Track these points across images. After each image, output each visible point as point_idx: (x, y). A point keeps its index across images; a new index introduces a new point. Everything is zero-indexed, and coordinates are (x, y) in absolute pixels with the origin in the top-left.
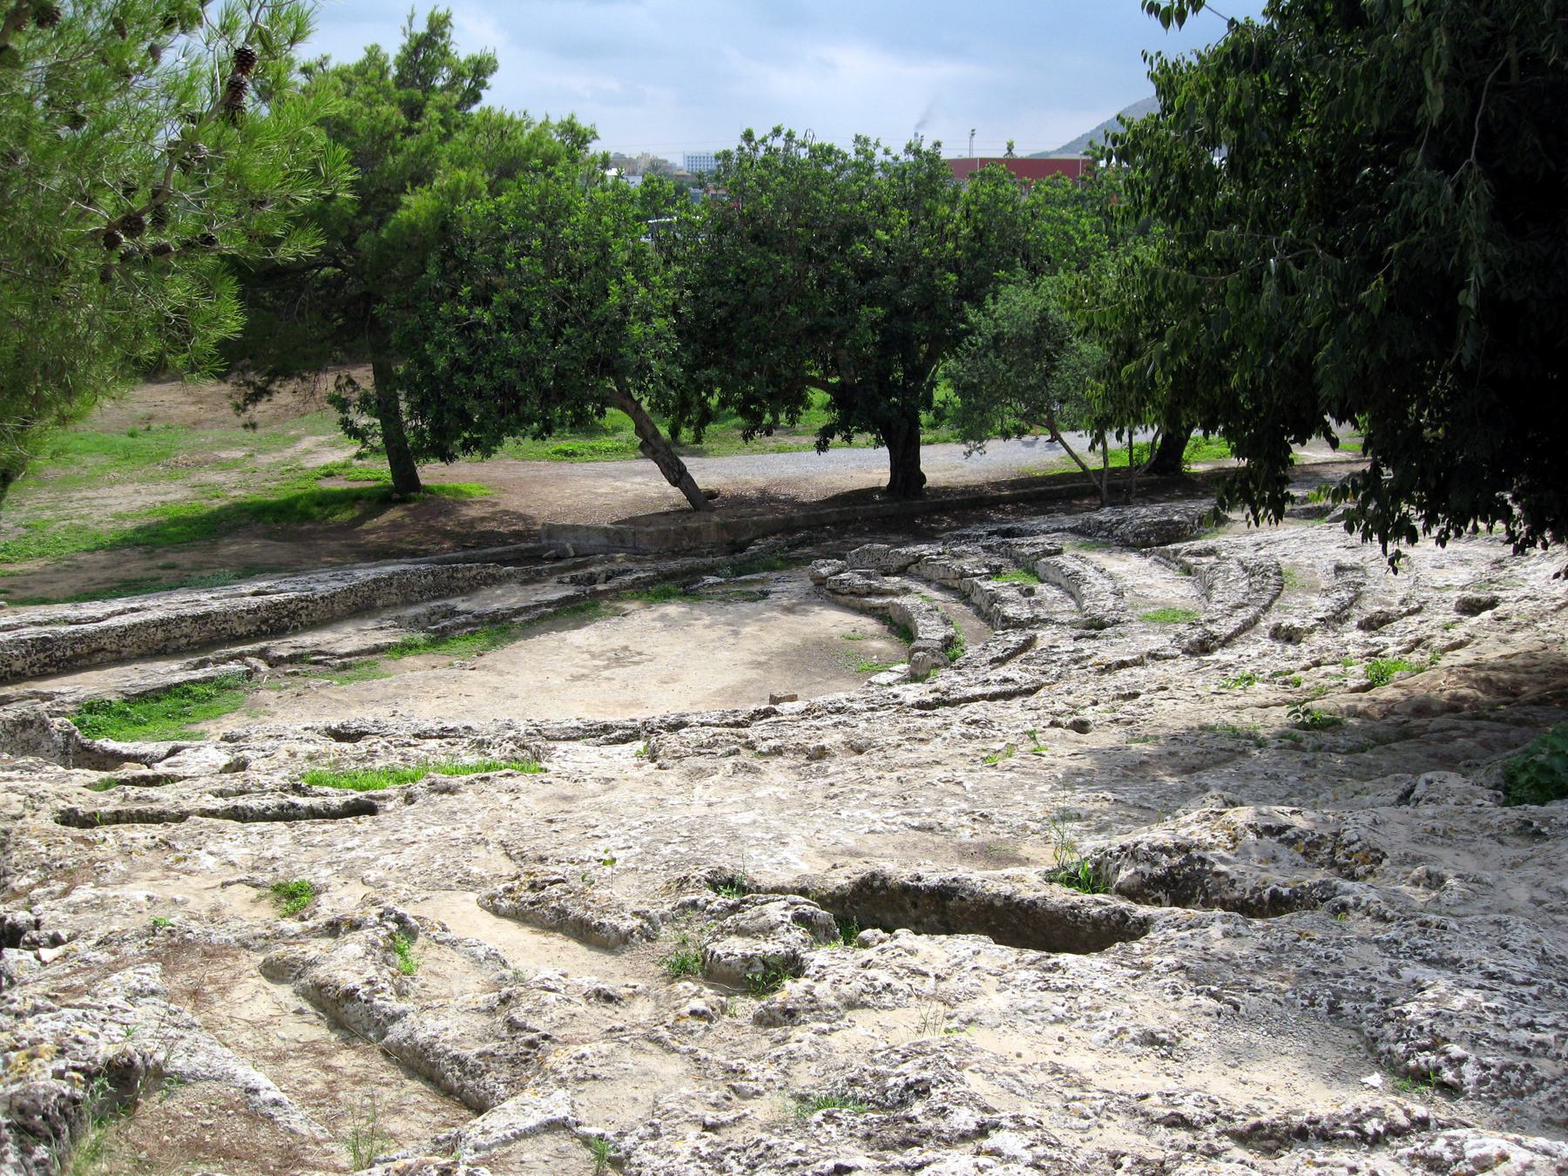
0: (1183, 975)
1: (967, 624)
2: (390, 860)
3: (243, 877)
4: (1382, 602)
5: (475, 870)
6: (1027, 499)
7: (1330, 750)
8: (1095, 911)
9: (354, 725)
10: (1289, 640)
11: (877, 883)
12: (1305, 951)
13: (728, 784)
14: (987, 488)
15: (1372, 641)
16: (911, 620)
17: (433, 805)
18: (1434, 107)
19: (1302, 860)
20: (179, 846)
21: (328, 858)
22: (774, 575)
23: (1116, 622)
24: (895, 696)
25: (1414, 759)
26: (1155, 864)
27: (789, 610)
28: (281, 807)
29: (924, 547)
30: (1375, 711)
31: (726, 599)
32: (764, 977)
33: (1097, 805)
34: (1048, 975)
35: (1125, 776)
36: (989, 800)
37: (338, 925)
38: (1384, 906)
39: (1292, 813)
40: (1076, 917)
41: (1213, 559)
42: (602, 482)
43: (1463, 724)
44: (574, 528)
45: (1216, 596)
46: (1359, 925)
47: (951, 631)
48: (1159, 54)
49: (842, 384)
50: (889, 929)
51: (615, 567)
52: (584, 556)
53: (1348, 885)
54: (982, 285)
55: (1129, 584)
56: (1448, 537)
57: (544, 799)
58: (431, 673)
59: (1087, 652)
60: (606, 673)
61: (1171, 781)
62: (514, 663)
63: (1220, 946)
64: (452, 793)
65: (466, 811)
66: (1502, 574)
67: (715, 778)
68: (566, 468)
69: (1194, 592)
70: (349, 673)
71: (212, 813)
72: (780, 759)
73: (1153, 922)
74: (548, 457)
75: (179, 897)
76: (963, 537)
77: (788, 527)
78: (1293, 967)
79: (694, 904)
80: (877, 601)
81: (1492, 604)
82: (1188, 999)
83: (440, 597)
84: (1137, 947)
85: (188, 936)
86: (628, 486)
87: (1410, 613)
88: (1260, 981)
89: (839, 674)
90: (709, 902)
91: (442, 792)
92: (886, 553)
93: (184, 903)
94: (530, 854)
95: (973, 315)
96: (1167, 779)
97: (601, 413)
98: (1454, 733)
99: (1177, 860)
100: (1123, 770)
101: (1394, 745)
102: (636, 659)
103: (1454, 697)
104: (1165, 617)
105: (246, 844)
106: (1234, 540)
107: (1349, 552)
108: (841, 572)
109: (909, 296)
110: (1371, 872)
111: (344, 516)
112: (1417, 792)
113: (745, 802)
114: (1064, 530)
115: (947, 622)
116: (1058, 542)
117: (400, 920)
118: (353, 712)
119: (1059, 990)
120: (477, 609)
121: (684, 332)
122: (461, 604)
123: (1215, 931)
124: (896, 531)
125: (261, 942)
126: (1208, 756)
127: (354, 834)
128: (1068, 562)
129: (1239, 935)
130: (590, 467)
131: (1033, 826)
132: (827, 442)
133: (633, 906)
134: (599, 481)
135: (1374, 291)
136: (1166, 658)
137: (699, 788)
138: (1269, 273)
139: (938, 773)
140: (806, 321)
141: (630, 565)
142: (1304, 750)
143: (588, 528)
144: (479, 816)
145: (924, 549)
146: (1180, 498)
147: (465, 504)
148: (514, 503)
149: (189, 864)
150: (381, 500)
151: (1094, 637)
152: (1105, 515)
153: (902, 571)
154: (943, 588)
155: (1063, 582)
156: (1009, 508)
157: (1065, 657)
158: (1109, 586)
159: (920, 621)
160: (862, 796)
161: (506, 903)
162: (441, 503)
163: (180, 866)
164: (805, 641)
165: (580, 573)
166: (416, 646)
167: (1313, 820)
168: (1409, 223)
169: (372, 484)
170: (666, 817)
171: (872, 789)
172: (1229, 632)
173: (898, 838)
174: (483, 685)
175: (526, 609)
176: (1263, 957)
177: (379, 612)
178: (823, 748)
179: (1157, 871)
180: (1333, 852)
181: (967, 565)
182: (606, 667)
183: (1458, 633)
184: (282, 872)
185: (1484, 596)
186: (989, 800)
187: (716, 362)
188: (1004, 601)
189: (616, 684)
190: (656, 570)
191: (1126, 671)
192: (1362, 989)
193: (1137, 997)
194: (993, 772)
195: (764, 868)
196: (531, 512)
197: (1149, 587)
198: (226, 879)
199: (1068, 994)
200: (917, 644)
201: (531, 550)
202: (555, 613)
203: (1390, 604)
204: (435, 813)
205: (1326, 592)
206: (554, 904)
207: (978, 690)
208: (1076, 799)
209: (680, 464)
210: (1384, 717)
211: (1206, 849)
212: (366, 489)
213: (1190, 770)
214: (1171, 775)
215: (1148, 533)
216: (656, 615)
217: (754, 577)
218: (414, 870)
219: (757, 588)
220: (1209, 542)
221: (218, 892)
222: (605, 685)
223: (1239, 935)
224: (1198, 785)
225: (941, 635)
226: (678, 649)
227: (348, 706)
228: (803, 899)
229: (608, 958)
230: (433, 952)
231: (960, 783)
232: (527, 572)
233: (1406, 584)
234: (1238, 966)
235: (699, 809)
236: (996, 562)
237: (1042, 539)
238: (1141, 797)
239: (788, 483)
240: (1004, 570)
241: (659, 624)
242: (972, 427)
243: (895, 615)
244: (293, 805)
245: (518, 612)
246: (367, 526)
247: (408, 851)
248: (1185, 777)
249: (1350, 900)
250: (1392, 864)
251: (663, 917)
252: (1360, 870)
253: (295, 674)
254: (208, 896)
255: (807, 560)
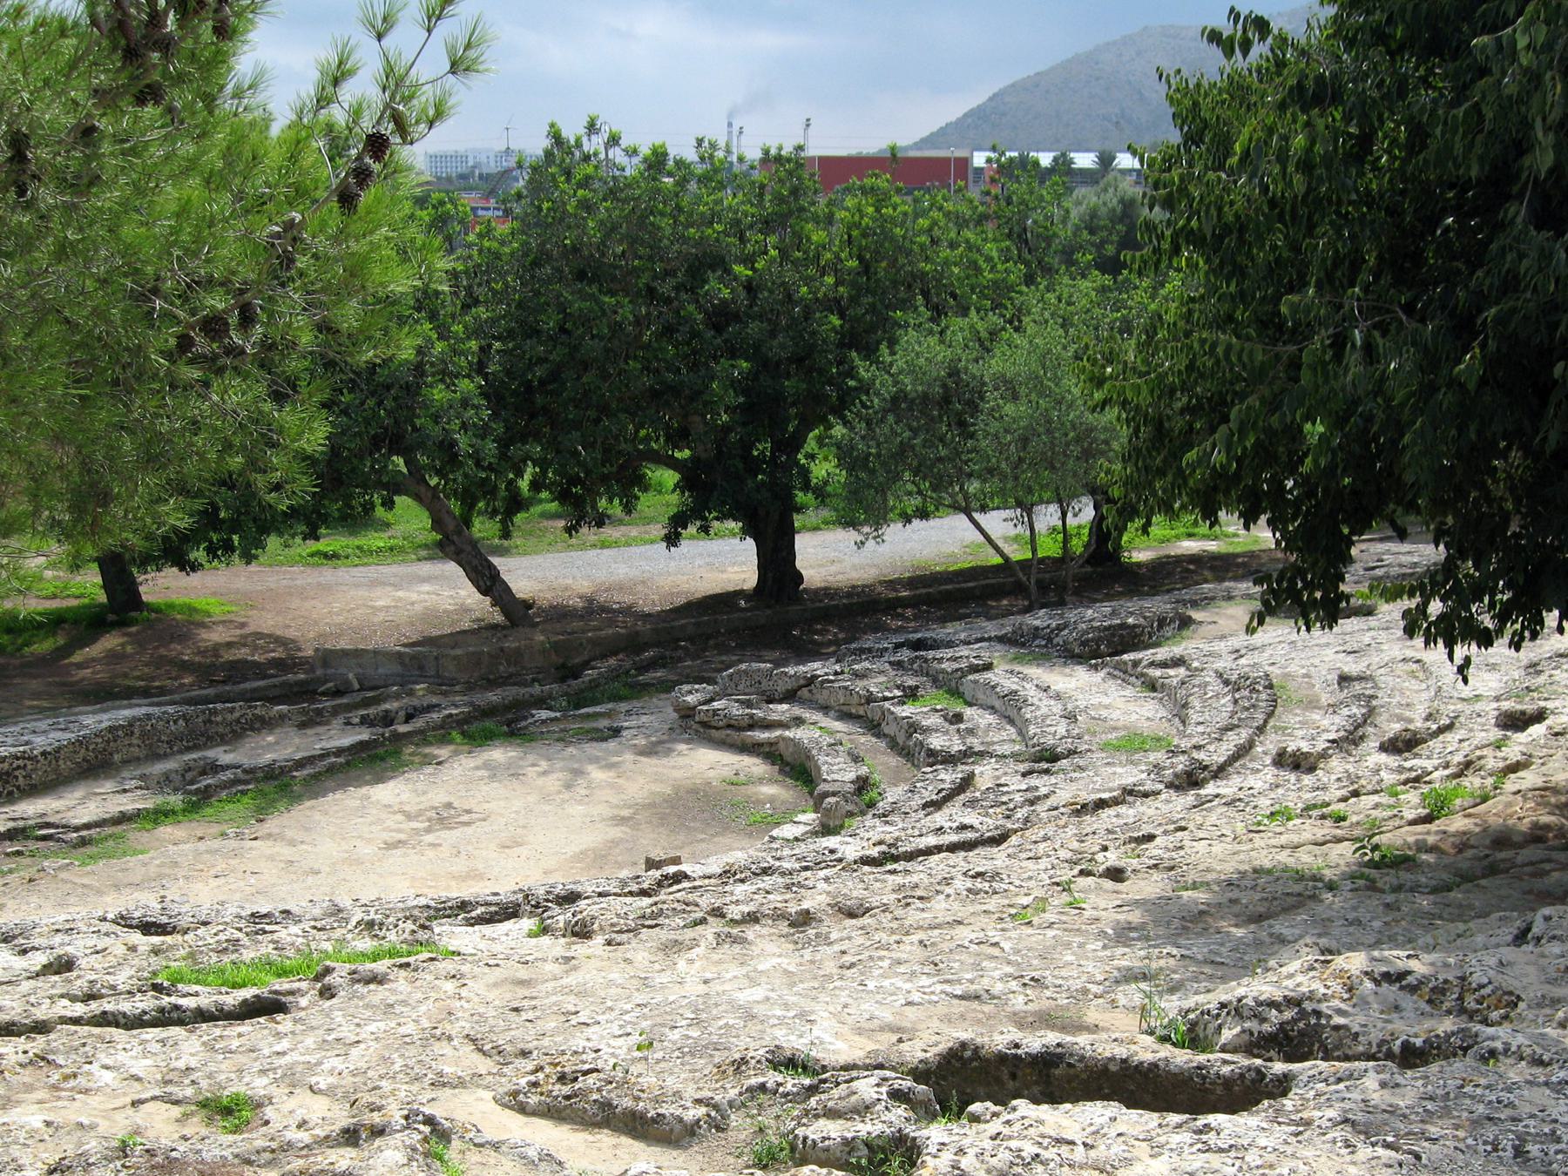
0: (1349, 1129)
1: (880, 761)
2: (338, 1063)
3: (157, 1092)
4: (1400, 718)
5: (447, 1070)
6: (930, 601)
7: (1412, 890)
8: (1226, 1070)
9: (137, 914)
10: (1296, 767)
11: (968, 1054)
12: (1472, 1097)
13: (715, 957)
14: (880, 589)
15: (1408, 764)
16: (809, 757)
17: (362, 998)
18: (1543, 159)
19: (1428, 1008)
20: (61, 1061)
21: (257, 1066)
22: (624, 706)
23: (1072, 753)
24: (832, 852)
25: (1508, 897)
26: (1264, 1020)
27: (650, 751)
28: (162, 1010)
29: (816, 665)
30: (1446, 846)
31: (564, 739)
32: (870, 1161)
33: (1162, 963)
34: (1204, 1137)
35: (1184, 928)
36: (1035, 962)
37: (355, 1131)
38: (1539, 1051)
39: (1408, 957)
40: (1204, 1078)
41: (1182, 671)
42: (378, 591)
43: (1555, 855)
44: (357, 653)
45: (1194, 717)
46: (1516, 1072)
47: (864, 771)
48: (1179, 71)
49: (693, 458)
50: (1002, 1101)
51: (416, 702)
52: (372, 689)
53: (1490, 1031)
54: (872, 329)
55: (1082, 704)
56: (1522, 639)
57: (495, 985)
58: (202, 846)
59: (1043, 791)
60: (429, 838)
61: (1239, 932)
62: (307, 829)
63: (1378, 1097)
64: (381, 983)
65: (404, 1003)
66: (1541, 679)
67: (697, 950)
68: (328, 574)
69: (1163, 713)
70: (89, 850)
71: (76, 1021)
72: (757, 927)
73: (1294, 1077)
74: (302, 561)
75: (86, 1122)
76: (862, 651)
77: (631, 644)
78: (1465, 1114)
79: (762, 1087)
80: (763, 736)
81: (1540, 716)
82: (1364, 1152)
83: (196, 748)
84: (1288, 1103)
85: (174, 1154)
86: (414, 597)
87: (1442, 730)
88: (1433, 1130)
89: (726, 829)
90: (780, 1084)
91: (368, 982)
92: (769, 675)
93: (93, 1127)
94: (508, 1048)
95: (864, 370)
96: (1233, 930)
97: (389, 504)
98: (1547, 866)
99: (1288, 1015)
100: (1179, 921)
101: (1483, 882)
102: (465, 818)
103: (1536, 826)
104: (1132, 744)
105: (146, 1054)
106: (1206, 647)
107: (1350, 658)
108: (712, 700)
109: (783, 347)
110: (1506, 1017)
111: (44, 646)
112: (1535, 930)
113: (747, 976)
114: (990, 639)
115: (856, 759)
116: (985, 655)
117: (430, 1121)
118: (108, 899)
119: (1221, 1150)
120: (247, 762)
121: (494, 395)
122: (223, 755)
123: (1371, 1082)
124: (771, 646)
125: (267, 1156)
126: (1272, 905)
127: (278, 1036)
128: (1002, 677)
129: (1397, 1085)
130: (372, 572)
131: (1094, 988)
132: (678, 535)
133: (690, 1092)
134: (387, 591)
135: (1469, 363)
136: (1146, 795)
137: (682, 965)
138: (1354, 345)
139: (964, 934)
140: (647, 381)
141: (435, 700)
142: (1383, 891)
143: (376, 652)
144: (423, 1008)
145: (816, 667)
146: (1120, 595)
147: (202, 625)
148: (266, 622)
149: (81, 1081)
150: (91, 623)
151: (1047, 772)
152: (1040, 619)
153: (790, 697)
154: (845, 716)
155: (997, 704)
156: (909, 612)
157: (1018, 798)
158: (1057, 708)
159: (822, 759)
160: (886, 964)
161: (533, 1100)
162: (173, 627)
163: (69, 1084)
164: (677, 789)
165: (372, 711)
166: (174, 812)
167: (1432, 964)
168: (1511, 284)
169: (74, 603)
170: (659, 998)
171: (894, 955)
172: (1222, 759)
173: (941, 1009)
174: (271, 858)
175: (310, 760)
176: (1430, 1106)
177: (118, 770)
178: (807, 912)
179: (1266, 1028)
180: (1461, 998)
181: (874, 685)
182: (428, 830)
183: (1513, 752)
184: (204, 1084)
185: (1529, 707)
186: (1035, 962)
187: (537, 436)
188: (926, 730)
189: (445, 851)
190: (472, 704)
191: (1111, 811)
192: (1546, 1130)
193: (1308, 1153)
194: (1030, 931)
195: (835, 1044)
196: (291, 633)
197: (1106, 707)
198: (136, 1097)
199: (1233, 1154)
200: (823, 787)
201: (304, 683)
202: (348, 763)
203: (1411, 721)
204: (367, 1006)
205: (1333, 708)
206: (595, 1096)
207: (932, 840)
208: (1129, 957)
209: (491, 566)
210: (1460, 851)
211: (1319, 1001)
212: (69, 609)
213: (1258, 919)
214: (1236, 926)
215: (1098, 641)
216: (479, 762)
217: (598, 709)
218: (370, 1074)
219: (603, 723)
220: (1177, 650)
221: (130, 1111)
222: (430, 853)
223: (1397, 1085)
224: (1271, 935)
225: (852, 776)
226: (517, 804)
227: (100, 893)
228: (893, 1075)
229: (675, 1153)
230: (474, 1156)
231: (996, 944)
232: (304, 712)
233: (1425, 695)
234: (1405, 1116)
235: (694, 989)
236: (911, 682)
237: (964, 651)
238: (1210, 951)
239: (621, 588)
240: (921, 692)
241: (484, 773)
242: (863, 508)
243: (788, 754)
244: (177, 1007)
245: (300, 764)
246: (77, 657)
247: (355, 1052)
248: (1252, 927)
249: (1498, 1045)
250: (1529, 1007)
251: (731, 1104)
252: (1495, 1015)
253: (19, 853)
254: (119, 1117)
255: (667, 687)
